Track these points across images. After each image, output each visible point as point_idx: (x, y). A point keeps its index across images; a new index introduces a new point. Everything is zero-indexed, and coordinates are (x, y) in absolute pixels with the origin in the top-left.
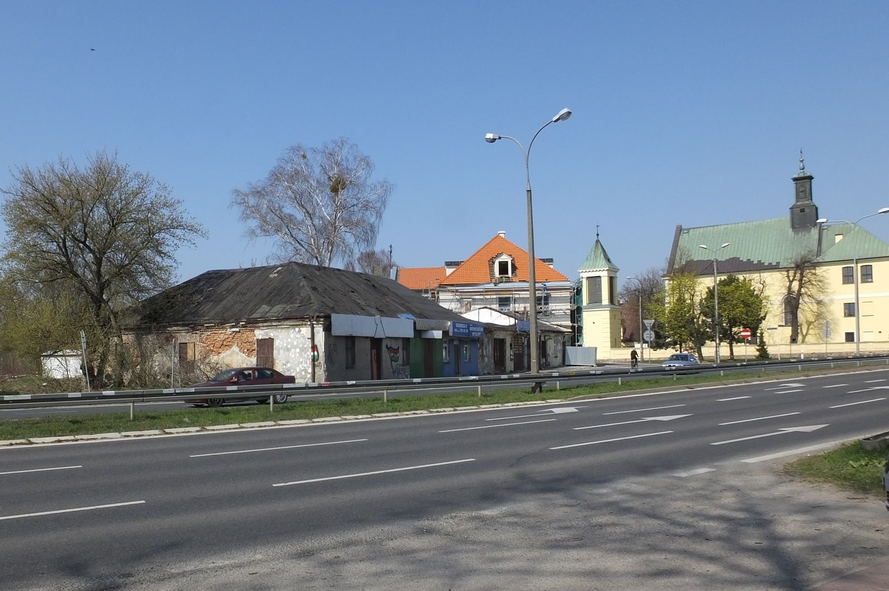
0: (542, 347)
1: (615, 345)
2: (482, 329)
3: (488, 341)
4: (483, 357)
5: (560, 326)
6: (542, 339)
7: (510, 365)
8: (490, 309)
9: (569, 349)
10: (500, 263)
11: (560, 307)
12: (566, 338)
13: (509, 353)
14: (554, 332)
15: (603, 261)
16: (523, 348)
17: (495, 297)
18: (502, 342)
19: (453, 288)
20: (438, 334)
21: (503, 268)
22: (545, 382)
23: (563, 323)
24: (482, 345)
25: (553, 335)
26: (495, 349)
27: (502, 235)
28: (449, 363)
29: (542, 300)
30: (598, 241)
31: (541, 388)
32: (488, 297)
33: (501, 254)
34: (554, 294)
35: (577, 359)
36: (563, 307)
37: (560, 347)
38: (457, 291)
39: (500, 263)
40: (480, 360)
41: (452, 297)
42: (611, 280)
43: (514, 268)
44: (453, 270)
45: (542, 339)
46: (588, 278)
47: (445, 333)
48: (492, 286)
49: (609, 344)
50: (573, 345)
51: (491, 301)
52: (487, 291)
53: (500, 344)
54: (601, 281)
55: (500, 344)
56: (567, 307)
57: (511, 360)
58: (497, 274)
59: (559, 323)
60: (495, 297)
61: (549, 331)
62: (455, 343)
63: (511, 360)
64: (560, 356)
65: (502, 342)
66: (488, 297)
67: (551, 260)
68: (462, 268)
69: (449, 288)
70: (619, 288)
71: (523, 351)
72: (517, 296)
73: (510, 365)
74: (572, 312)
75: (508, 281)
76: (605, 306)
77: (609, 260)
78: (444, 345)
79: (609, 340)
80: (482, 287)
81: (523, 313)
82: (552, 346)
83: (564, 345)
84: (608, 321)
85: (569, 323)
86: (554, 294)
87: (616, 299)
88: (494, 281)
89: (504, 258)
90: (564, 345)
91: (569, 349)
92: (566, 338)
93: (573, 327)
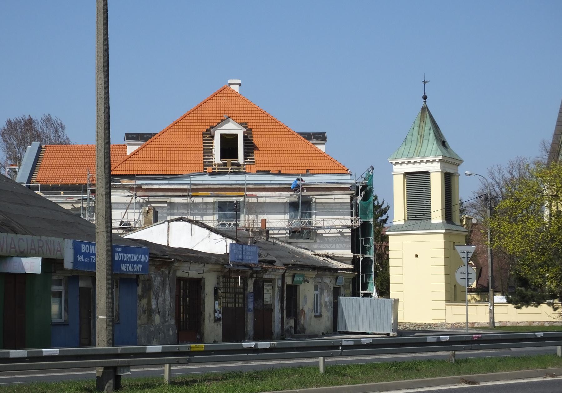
0: (290, 295)
1: (454, 295)
2: (145, 258)
3: (163, 283)
4: (150, 313)
5: (333, 258)
6: (288, 281)
7: (212, 329)
8: (191, 221)
9: (345, 301)
10: (223, 136)
11: (334, 222)
12: (341, 281)
13: (211, 306)
14: (314, 268)
15: (432, 145)
16: (245, 297)
17: (211, 200)
18: (197, 285)
19: (132, 182)
20: (32, 265)
21: (229, 146)
22: (128, 367)
23: (339, 253)
24: (148, 289)
25: (313, 274)
26: (178, 300)
27: (236, 88)
28: (65, 324)
29: (303, 206)
30: (425, 109)
31: (117, 379)
32: (198, 200)
33: (223, 121)
34: (319, 198)
35: (361, 316)
36: (337, 223)
37: (327, 298)
38: (139, 188)
39: (223, 136)
40: (144, 318)
41: (128, 200)
42: (448, 180)
43: (250, 146)
44: (136, 148)
45: (288, 281)
46: (406, 174)
47: (51, 264)
48: (206, 179)
49: (443, 295)
50: (355, 294)
51: (204, 209)
52: (196, 190)
53: (190, 292)
54: (428, 181)
55: (190, 292)
56: (344, 221)
57: (217, 320)
58: (217, 158)
59: (330, 252)
60: (211, 200)
61: (303, 267)
62: (82, 284)
63: (217, 320)
64: (327, 314)
65: (197, 285)
66: (198, 200)
67: (321, 137)
68: (153, 145)
69: (125, 182)
70: (467, 191)
71: (245, 304)
72: (253, 200)
73: (212, 329)
74: (354, 232)
75: (238, 170)
76: (436, 226)
77: (443, 144)
78: (55, 288)
79: (443, 287)
80: (187, 181)
81: (260, 232)
82: (308, 293)
83: (337, 292)
84: (442, 253)
85: (348, 253)
86: (319, 198)
87: (456, 216)
88: (209, 169)
89: (231, 128)
90: (337, 292)
91: (345, 301)
92: (341, 281)
93: (354, 261)
